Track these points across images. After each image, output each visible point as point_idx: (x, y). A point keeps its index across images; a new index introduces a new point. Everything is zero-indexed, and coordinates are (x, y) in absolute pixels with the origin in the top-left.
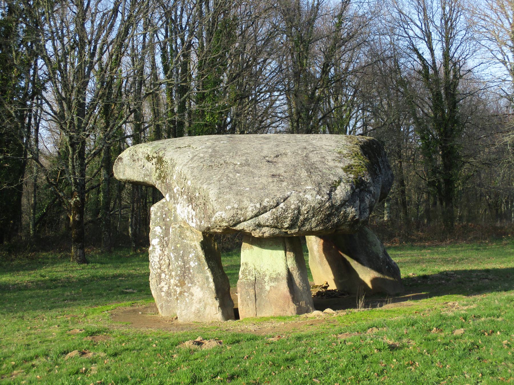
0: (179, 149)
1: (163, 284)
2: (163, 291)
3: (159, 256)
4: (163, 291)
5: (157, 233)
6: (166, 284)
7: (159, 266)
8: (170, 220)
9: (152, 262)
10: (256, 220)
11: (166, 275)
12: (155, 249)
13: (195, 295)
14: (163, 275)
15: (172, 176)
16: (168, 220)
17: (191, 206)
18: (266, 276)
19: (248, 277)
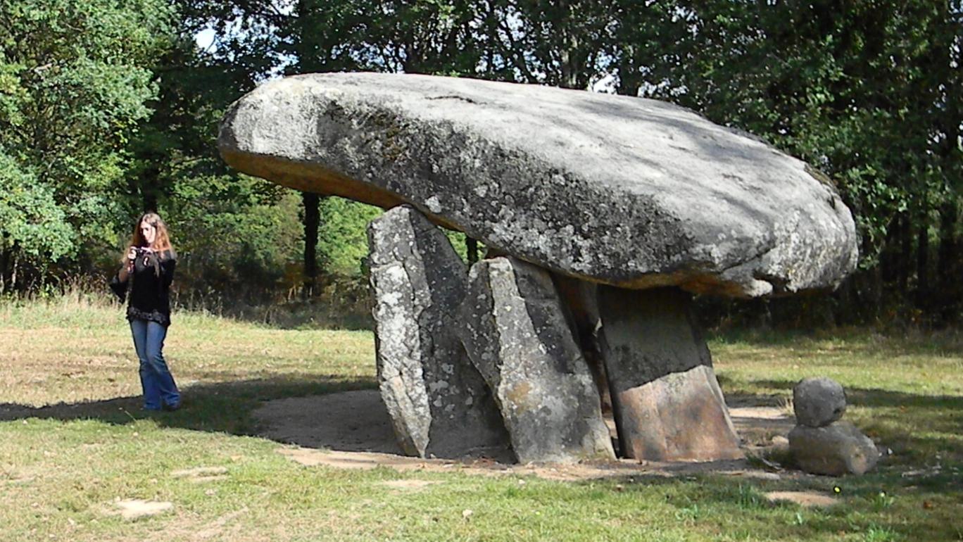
3: (404, 330)
7: (406, 350)
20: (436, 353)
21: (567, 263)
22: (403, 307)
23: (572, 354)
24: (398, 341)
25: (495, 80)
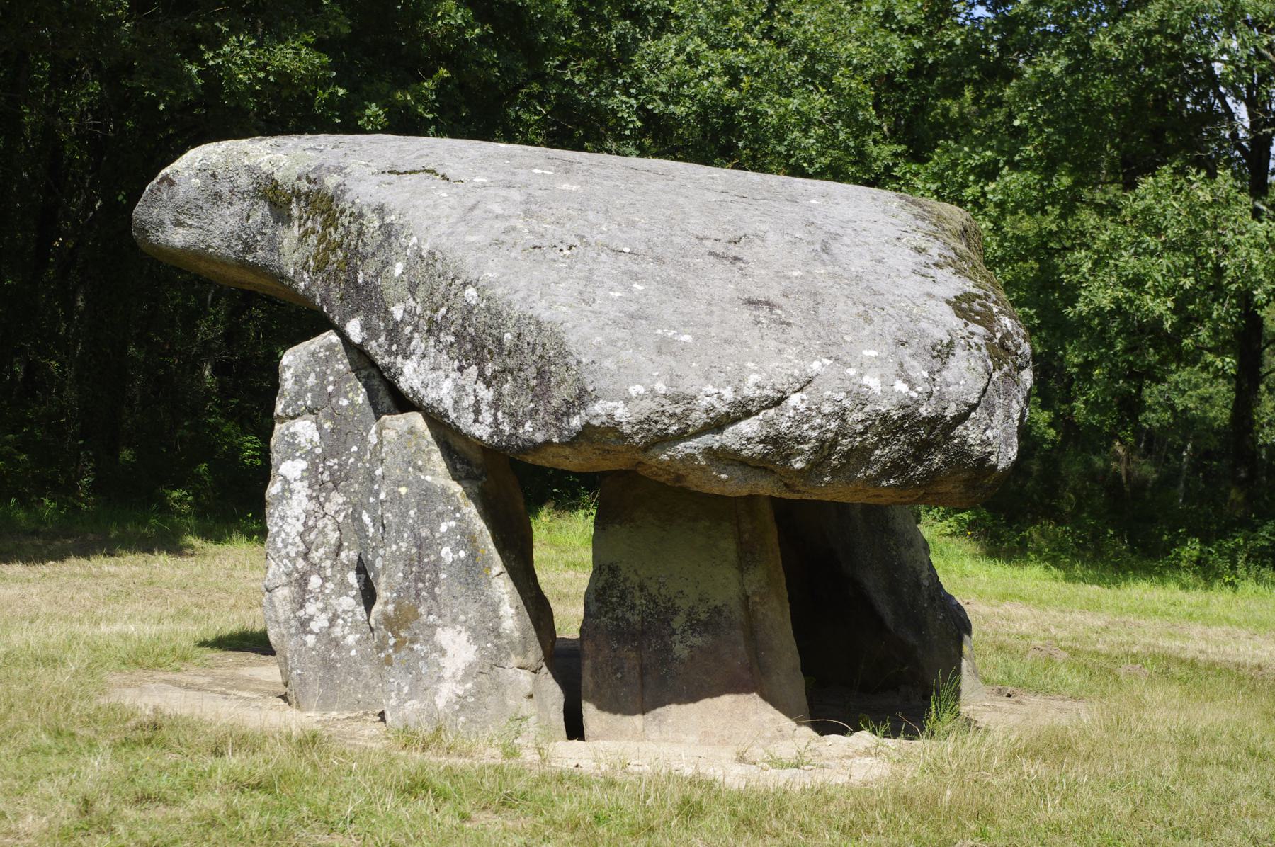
0: (394, 176)
1: (311, 608)
2: (311, 632)
3: (303, 518)
4: (311, 632)
5: (301, 440)
6: (324, 610)
7: (302, 548)
8: (352, 404)
9: (278, 533)
10: (714, 440)
11: (325, 579)
12: (291, 492)
13: (449, 653)
14: (315, 581)
15: (386, 264)
16: (344, 402)
17: (473, 370)
18: (676, 613)
19: (619, 613)
20: (343, 555)
21: (466, 423)
22: (306, 483)
23: (488, 564)
24: (293, 533)
25: (350, 127)
